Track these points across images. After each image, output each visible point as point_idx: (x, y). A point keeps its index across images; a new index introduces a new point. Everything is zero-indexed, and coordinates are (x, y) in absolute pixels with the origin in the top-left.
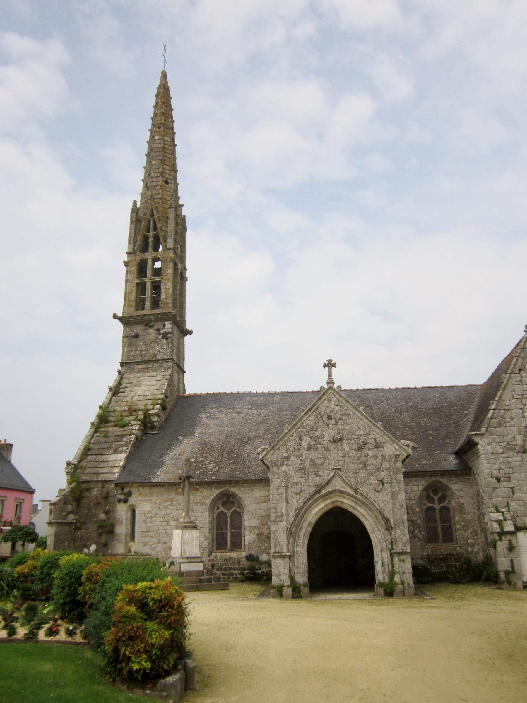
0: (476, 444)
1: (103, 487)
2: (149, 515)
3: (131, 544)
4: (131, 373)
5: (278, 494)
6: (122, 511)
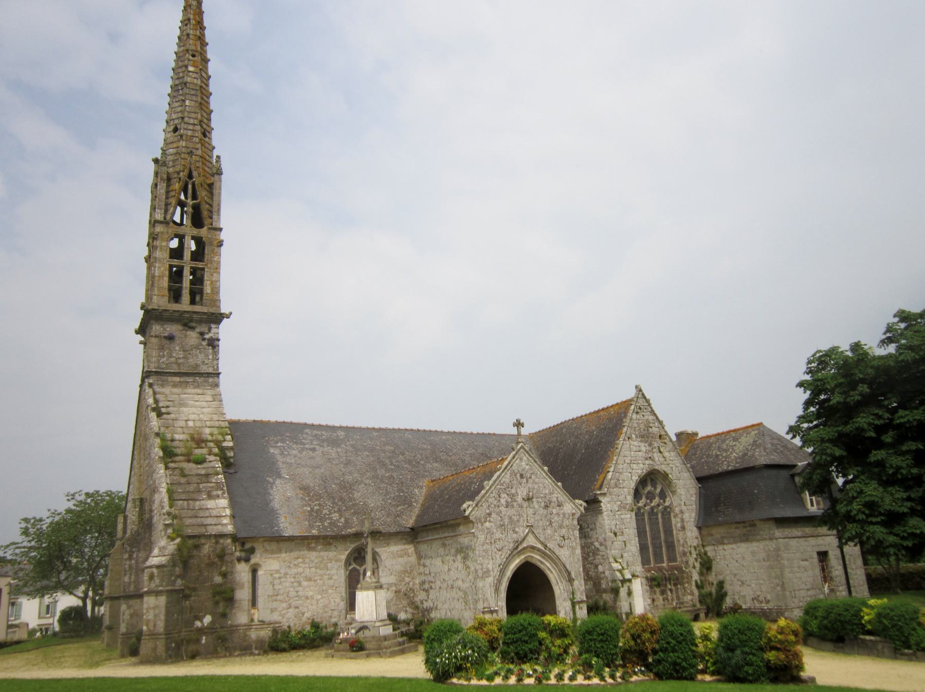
0: (600, 502)
1: (217, 543)
2: (277, 576)
3: (253, 611)
4: (162, 386)
5: (484, 551)
6: (242, 571)
